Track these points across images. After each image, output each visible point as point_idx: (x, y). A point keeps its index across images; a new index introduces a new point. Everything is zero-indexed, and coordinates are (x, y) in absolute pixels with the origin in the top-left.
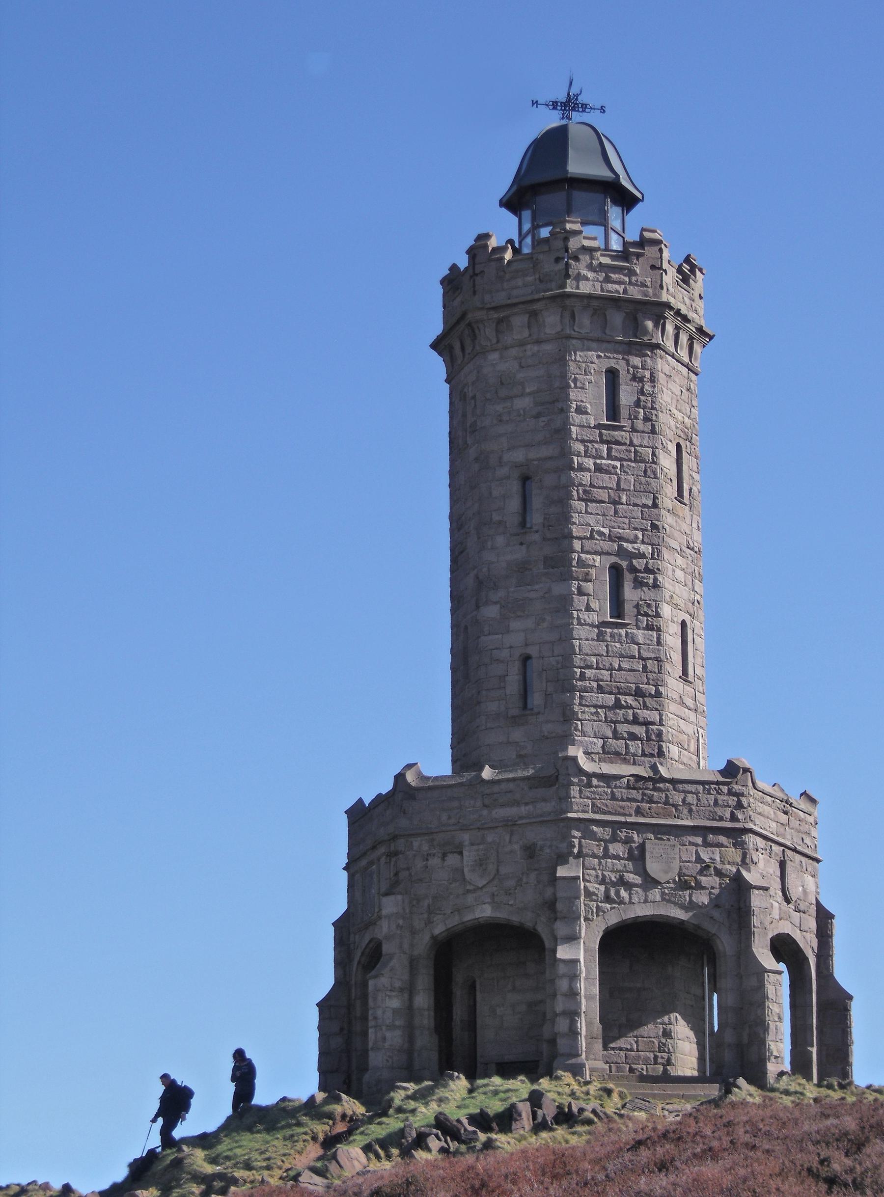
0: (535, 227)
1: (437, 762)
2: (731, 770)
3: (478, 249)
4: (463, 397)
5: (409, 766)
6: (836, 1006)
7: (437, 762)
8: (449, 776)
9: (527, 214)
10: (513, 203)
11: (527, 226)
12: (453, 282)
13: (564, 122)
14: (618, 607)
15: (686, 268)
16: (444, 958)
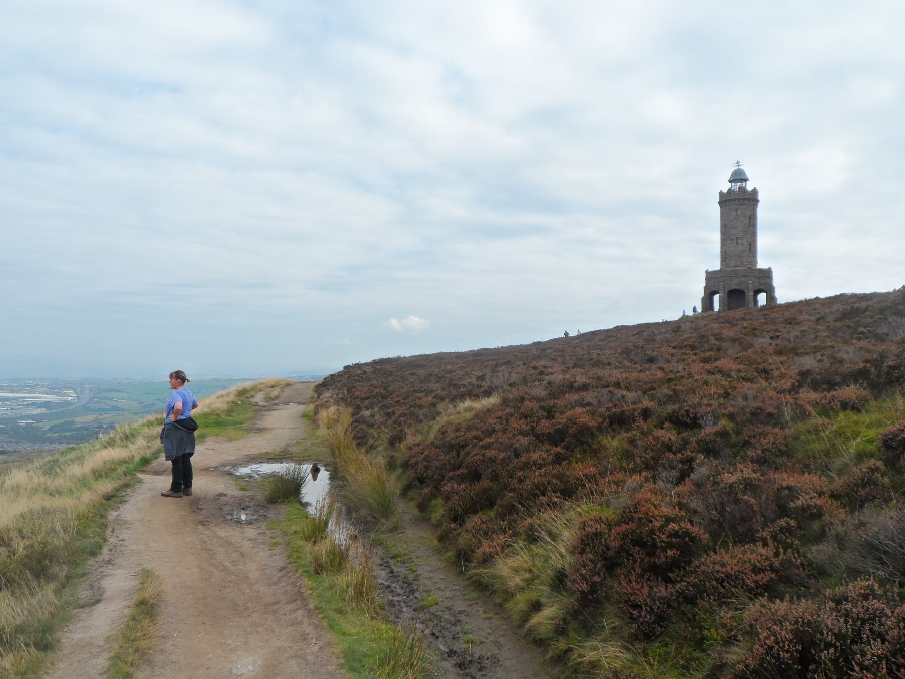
14: (737, 243)
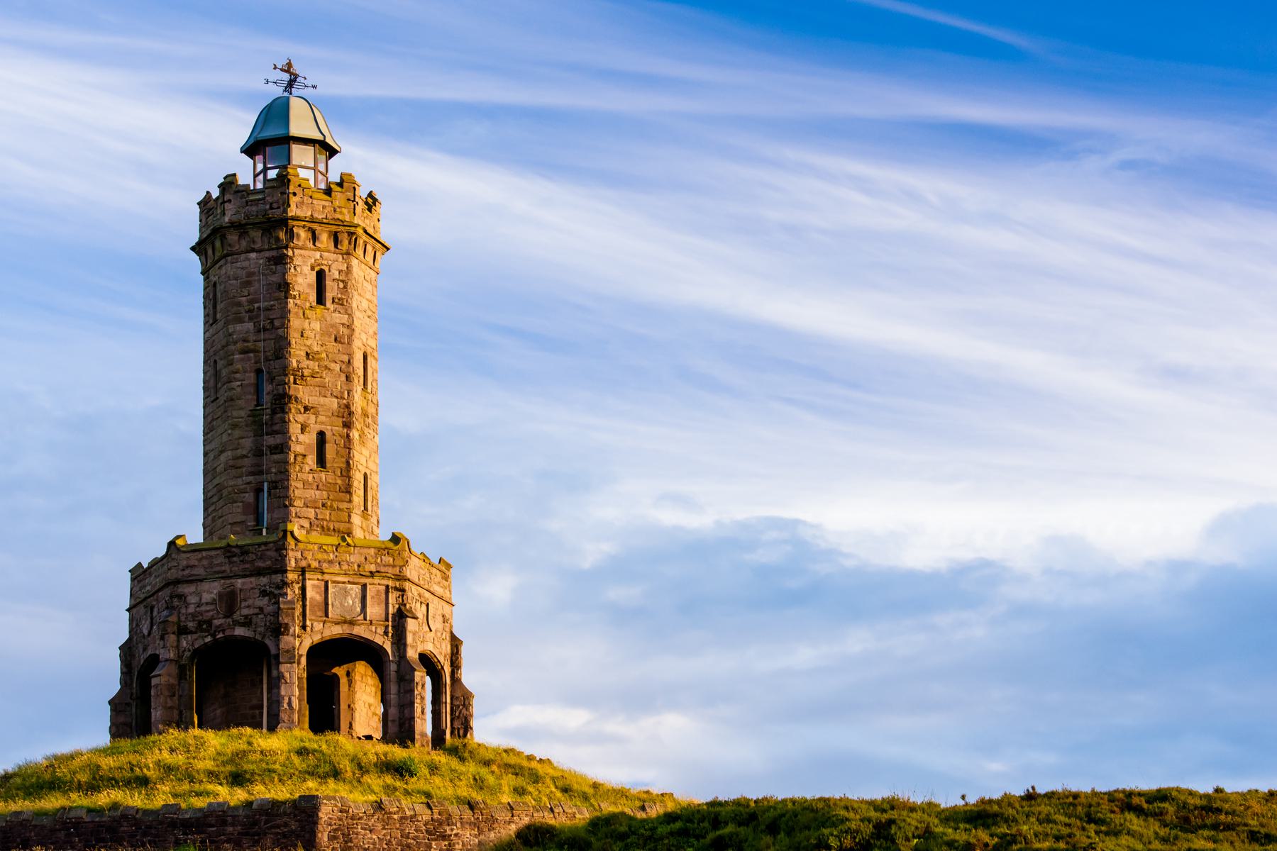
0: (265, 170)
1: (195, 535)
2: (395, 539)
3: (229, 184)
4: (773, 829)
5: (178, 537)
6: (463, 701)
7: (195, 535)
8: (104, 752)
9: (259, 158)
10: (251, 150)
11: (260, 167)
12: (206, 205)
13: (286, 94)
15: (370, 200)
16: (209, 636)
